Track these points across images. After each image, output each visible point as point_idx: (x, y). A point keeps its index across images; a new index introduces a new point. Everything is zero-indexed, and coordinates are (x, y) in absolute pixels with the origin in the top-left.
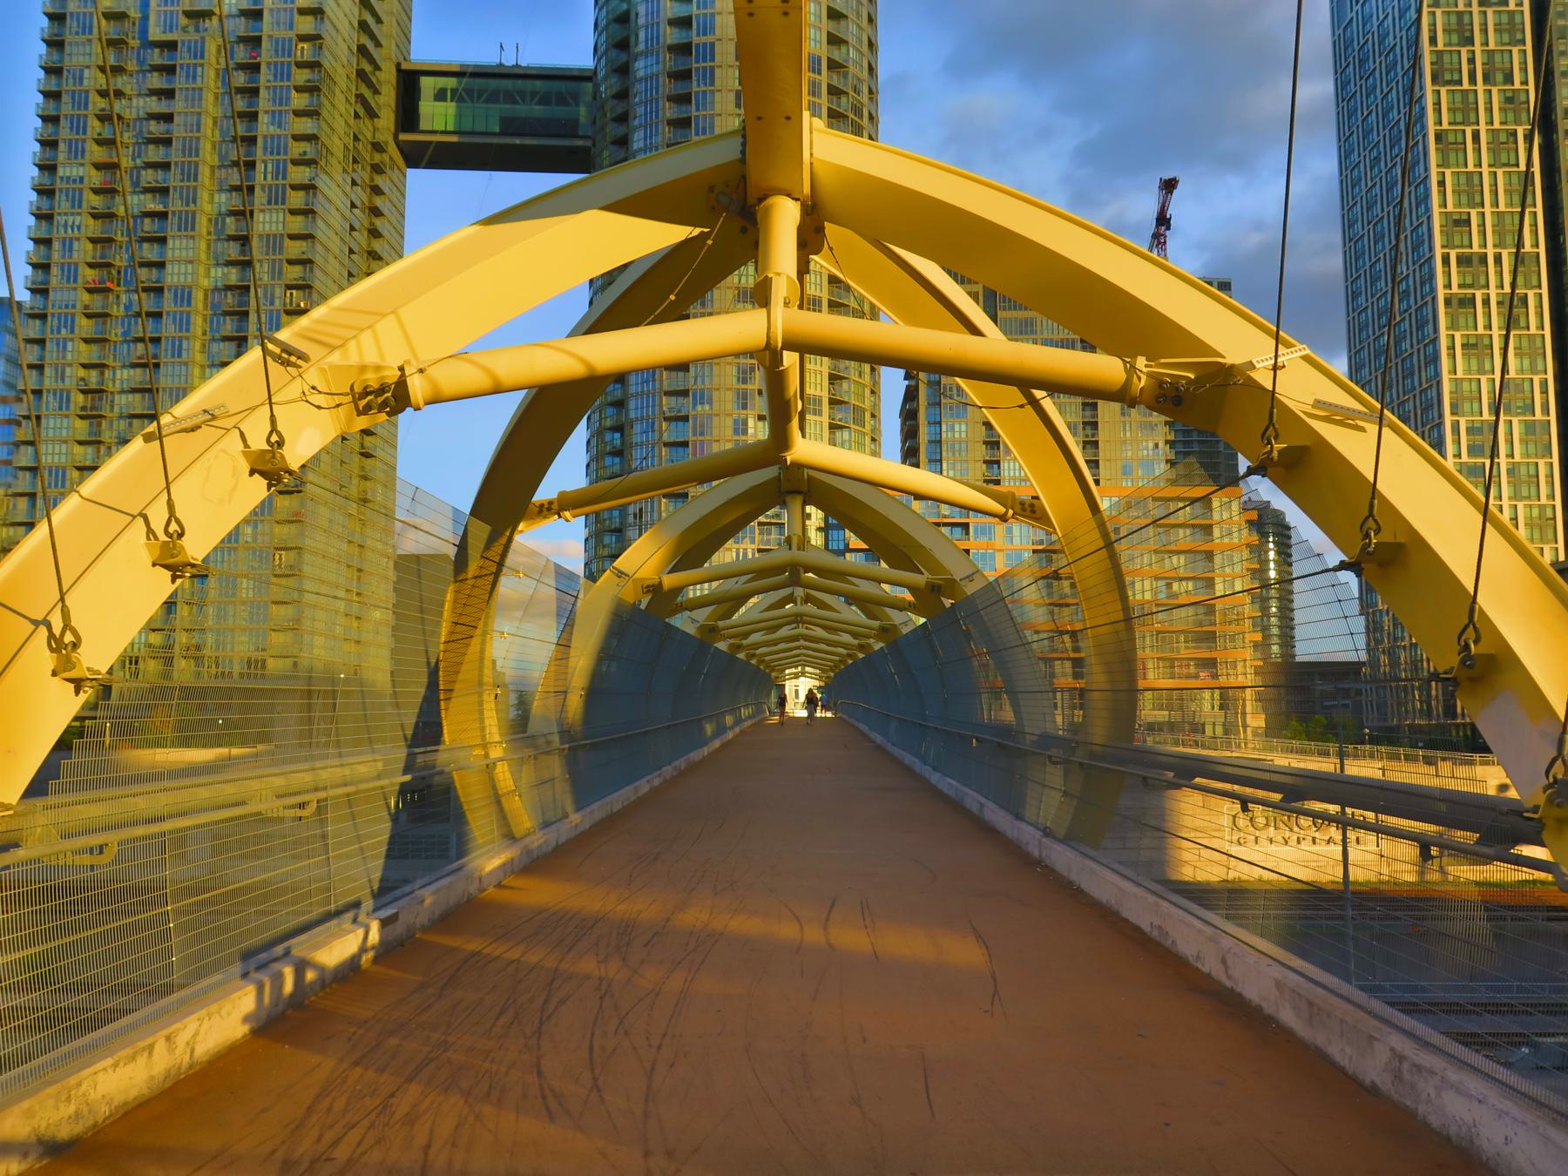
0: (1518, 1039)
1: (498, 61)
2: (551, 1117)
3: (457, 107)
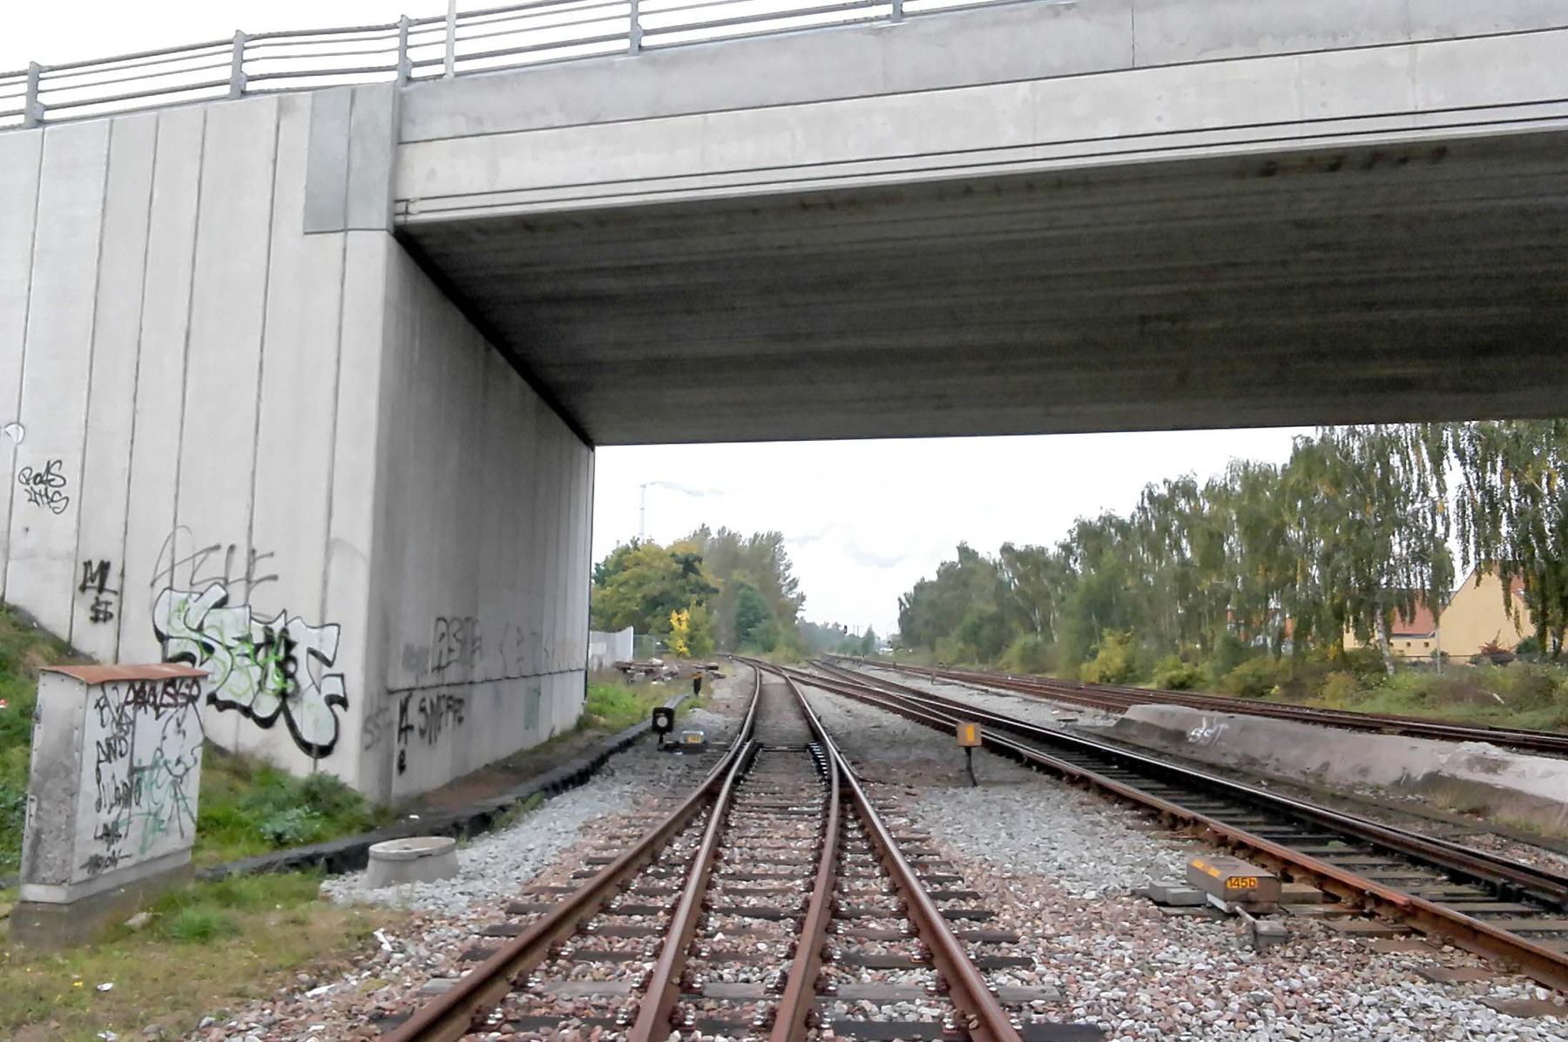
0: (1268, 713)
1: (385, 233)
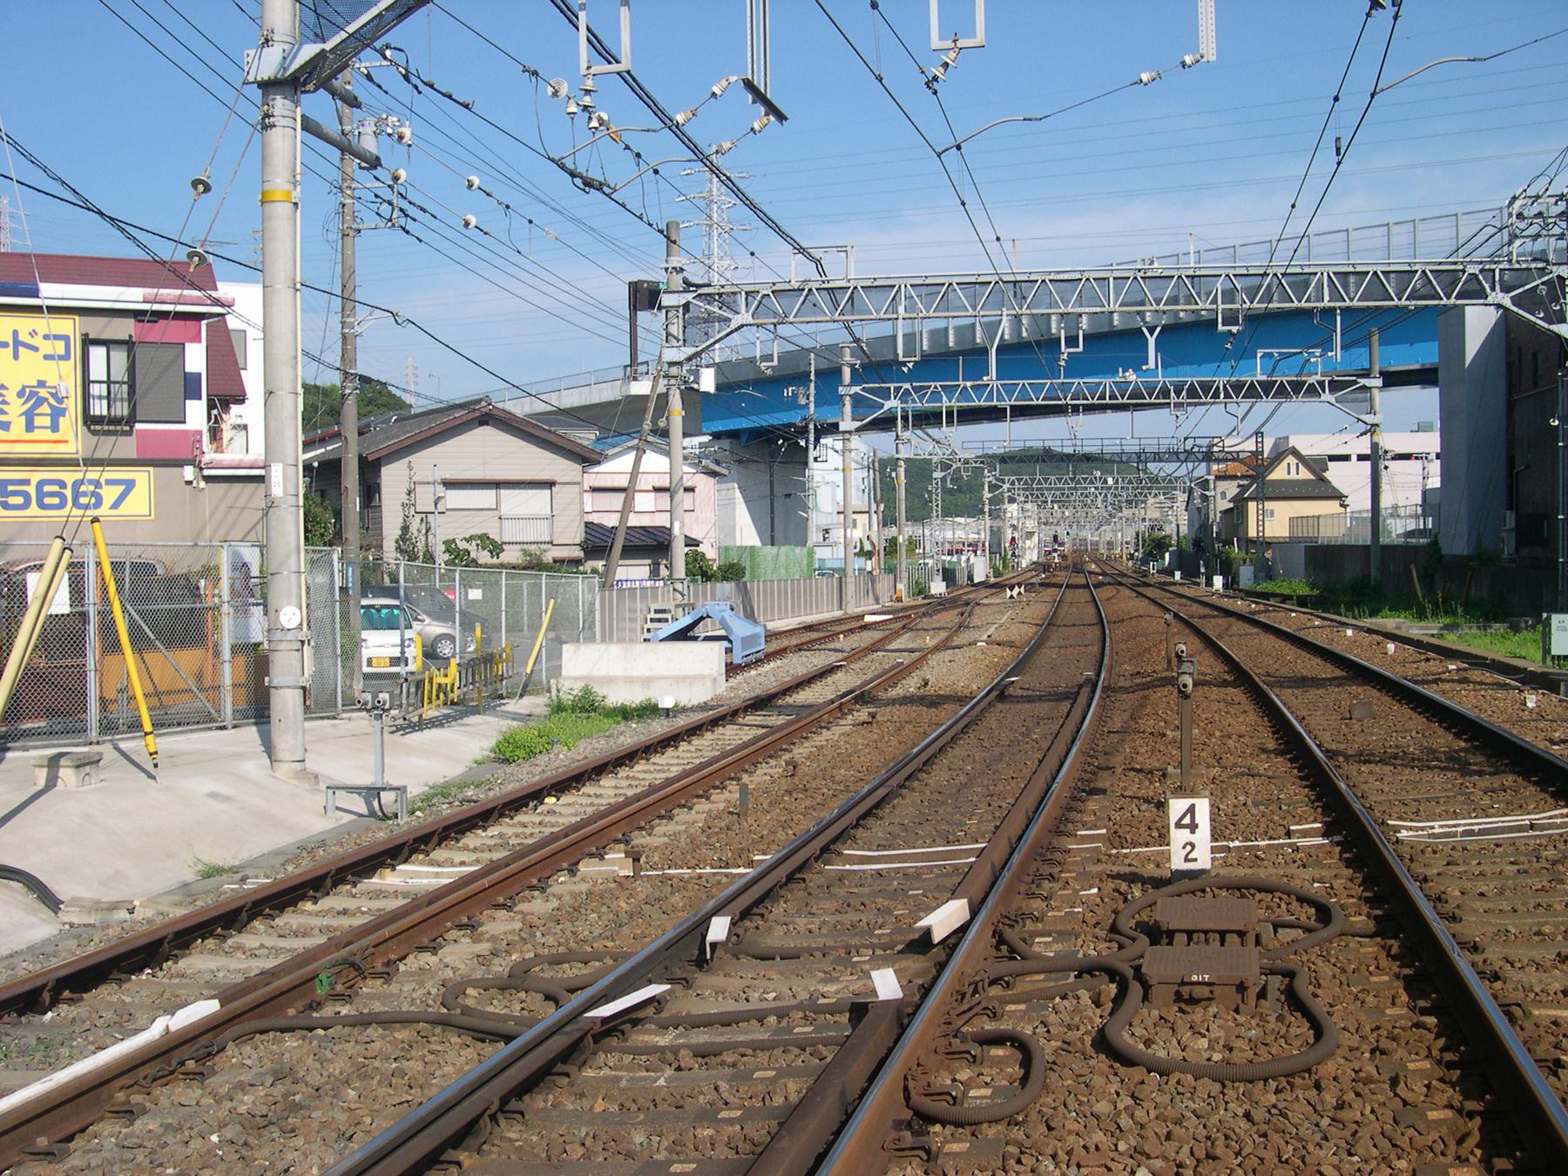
0: (762, 215)
2: (610, 63)
3: (259, 731)
